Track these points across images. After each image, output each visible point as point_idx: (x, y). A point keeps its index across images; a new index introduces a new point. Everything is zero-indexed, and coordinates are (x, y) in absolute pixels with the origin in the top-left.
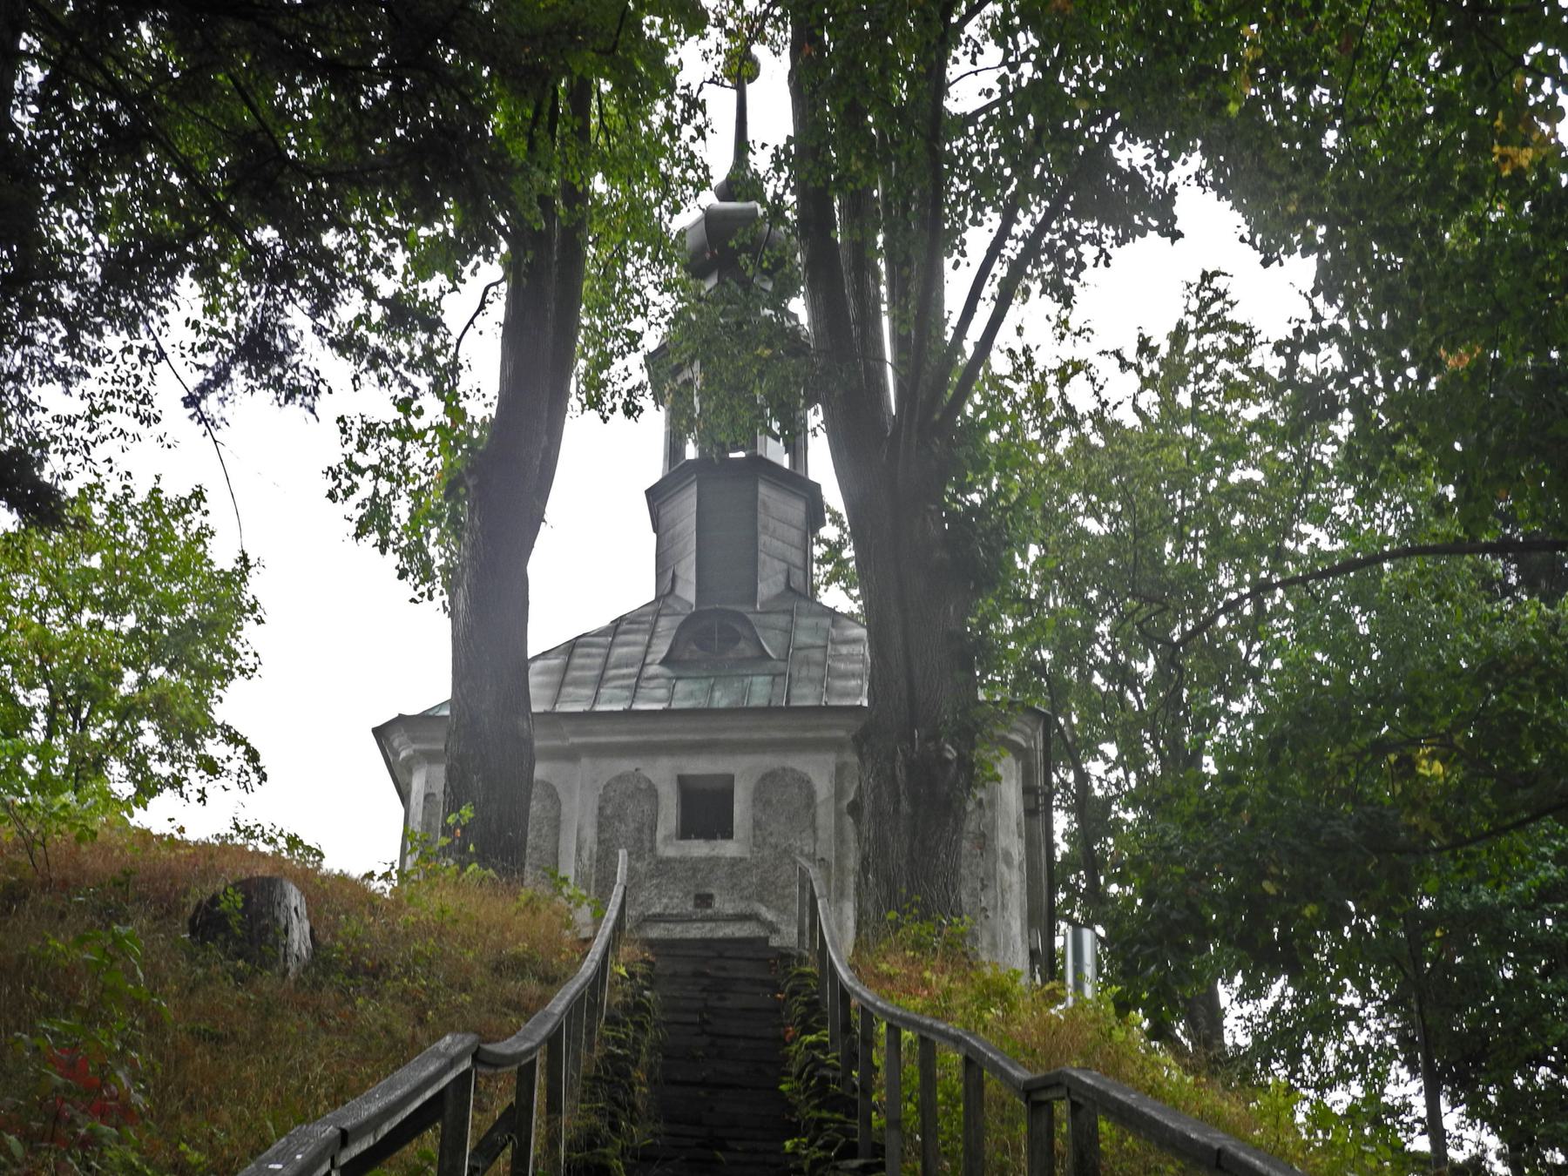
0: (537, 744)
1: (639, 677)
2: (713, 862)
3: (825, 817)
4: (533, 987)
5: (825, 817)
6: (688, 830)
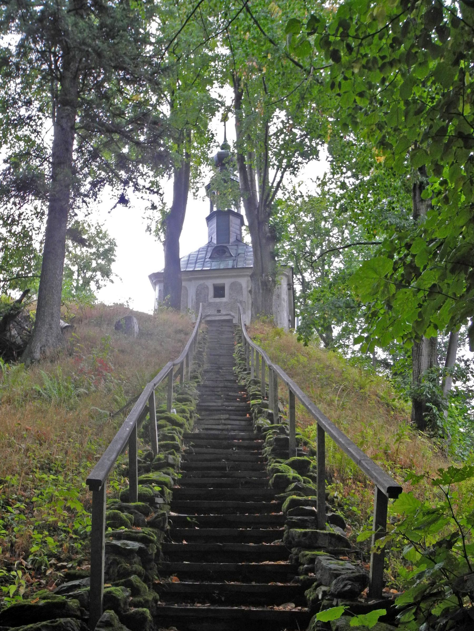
0: (182, 278)
1: (204, 261)
2: (221, 303)
3: (245, 292)
4: (183, 336)
5: (245, 292)
6: (216, 296)
